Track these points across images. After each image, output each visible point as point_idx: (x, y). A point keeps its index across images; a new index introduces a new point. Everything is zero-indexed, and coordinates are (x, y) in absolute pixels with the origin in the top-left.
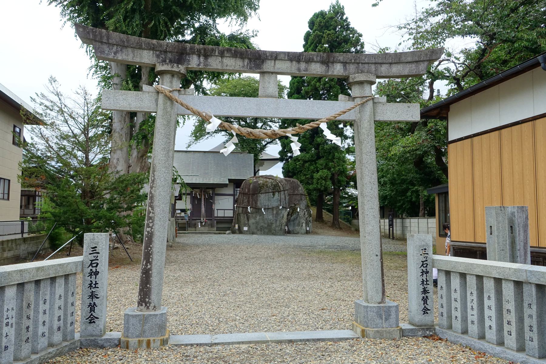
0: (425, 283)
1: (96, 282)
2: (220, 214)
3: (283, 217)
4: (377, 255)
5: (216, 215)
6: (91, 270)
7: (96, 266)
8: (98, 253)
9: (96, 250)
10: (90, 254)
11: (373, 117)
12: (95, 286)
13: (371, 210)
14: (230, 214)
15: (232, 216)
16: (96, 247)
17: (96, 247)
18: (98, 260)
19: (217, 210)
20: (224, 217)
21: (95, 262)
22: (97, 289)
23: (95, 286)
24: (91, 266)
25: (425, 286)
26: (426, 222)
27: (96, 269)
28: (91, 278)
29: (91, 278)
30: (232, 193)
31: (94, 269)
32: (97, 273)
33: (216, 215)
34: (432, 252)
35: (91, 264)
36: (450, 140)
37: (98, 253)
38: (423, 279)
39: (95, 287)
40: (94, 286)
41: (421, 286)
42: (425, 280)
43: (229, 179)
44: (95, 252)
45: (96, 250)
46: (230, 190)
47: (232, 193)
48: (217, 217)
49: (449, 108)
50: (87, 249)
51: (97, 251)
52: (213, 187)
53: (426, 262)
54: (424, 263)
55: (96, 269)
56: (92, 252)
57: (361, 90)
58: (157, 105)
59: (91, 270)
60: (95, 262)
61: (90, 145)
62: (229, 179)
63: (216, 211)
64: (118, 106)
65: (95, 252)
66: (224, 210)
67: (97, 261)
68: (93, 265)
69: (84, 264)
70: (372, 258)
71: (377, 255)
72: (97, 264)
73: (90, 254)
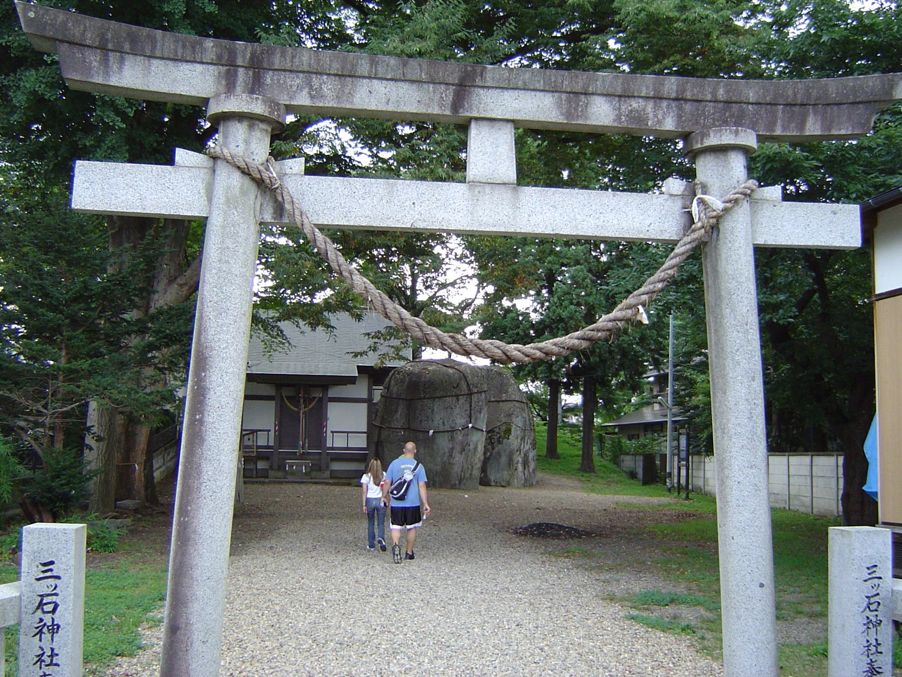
0: (873, 649)
1: (52, 650)
2: (339, 442)
3: (475, 449)
4: (762, 585)
5: (329, 444)
6: (41, 620)
7: (54, 611)
8: (58, 578)
9: (51, 570)
10: (38, 579)
11: (750, 237)
12: (52, 661)
13: (750, 471)
14: (360, 442)
15: (365, 446)
16: (52, 563)
17: (52, 563)
18: (56, 594)
19: (333, 432)
20: (347, 449)
21: (49, 599)
22: (55, 667)
23: (52, 661)
24: (40, 611)
25: (874, 658)
26: (806, 471)
27: (53, 619)
28: (40, 640)
29: (40, 640)
30: (365, 395)
31: (48, 619)
32: (55, 628)
33: (329, 444)
34: (890, 573)
35: (41, 605)
36: (878, 291)
37: (58, 578)
38: (868, 641)
39: (51, 664)
40: (48, 661)
41: (864, 658)
42: (874, 643)
43: (358, 366)
44: (49, 574)
45: (51, 570)
46: (361, 390)
47: (365, 395)
48: (333, 448)
49: (876, 219)
50: (30, 565)
51: (55, 573)
52: (325, 383)
53: (876, 599)
54: (872, 600)
55: (53, 619)
56: (42, 575)
57: (721, 169)
58: (210, 200)
59: (41, 620)
60: (49, 599)
61: (300, 13)
62: (358, 366)
63: (329, 434)
64: (113, 202)
65: (49, 574)
66: (348, 433)
67: (54, 598)
68: (46, 608)
69: (24, 604)
70: (749, 592)
71: (762, 585)
72: (56, 606)
73: (38, 579)
